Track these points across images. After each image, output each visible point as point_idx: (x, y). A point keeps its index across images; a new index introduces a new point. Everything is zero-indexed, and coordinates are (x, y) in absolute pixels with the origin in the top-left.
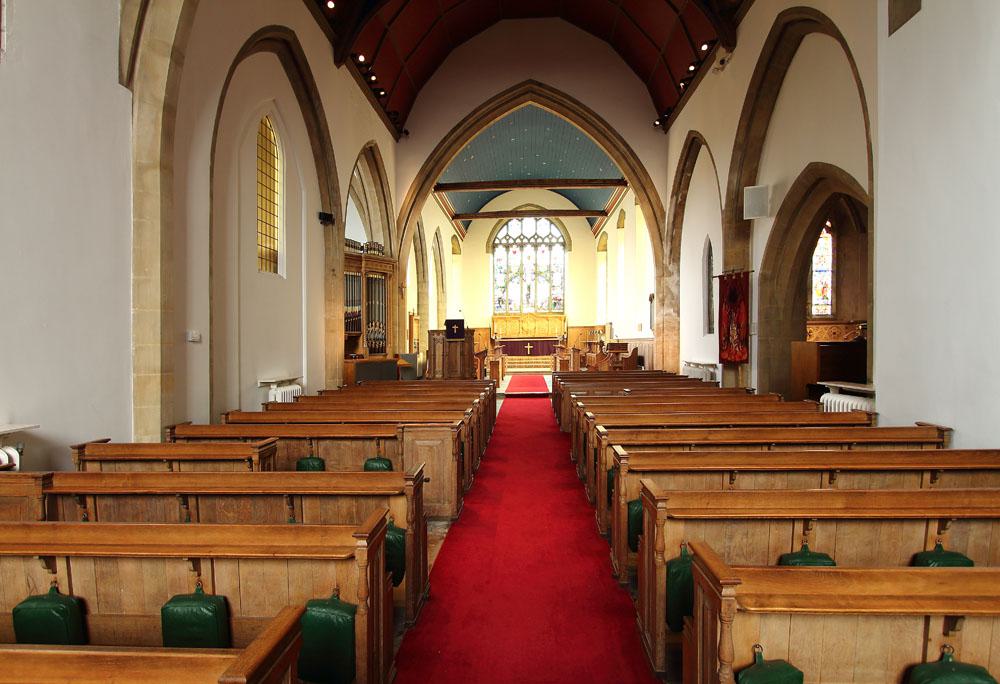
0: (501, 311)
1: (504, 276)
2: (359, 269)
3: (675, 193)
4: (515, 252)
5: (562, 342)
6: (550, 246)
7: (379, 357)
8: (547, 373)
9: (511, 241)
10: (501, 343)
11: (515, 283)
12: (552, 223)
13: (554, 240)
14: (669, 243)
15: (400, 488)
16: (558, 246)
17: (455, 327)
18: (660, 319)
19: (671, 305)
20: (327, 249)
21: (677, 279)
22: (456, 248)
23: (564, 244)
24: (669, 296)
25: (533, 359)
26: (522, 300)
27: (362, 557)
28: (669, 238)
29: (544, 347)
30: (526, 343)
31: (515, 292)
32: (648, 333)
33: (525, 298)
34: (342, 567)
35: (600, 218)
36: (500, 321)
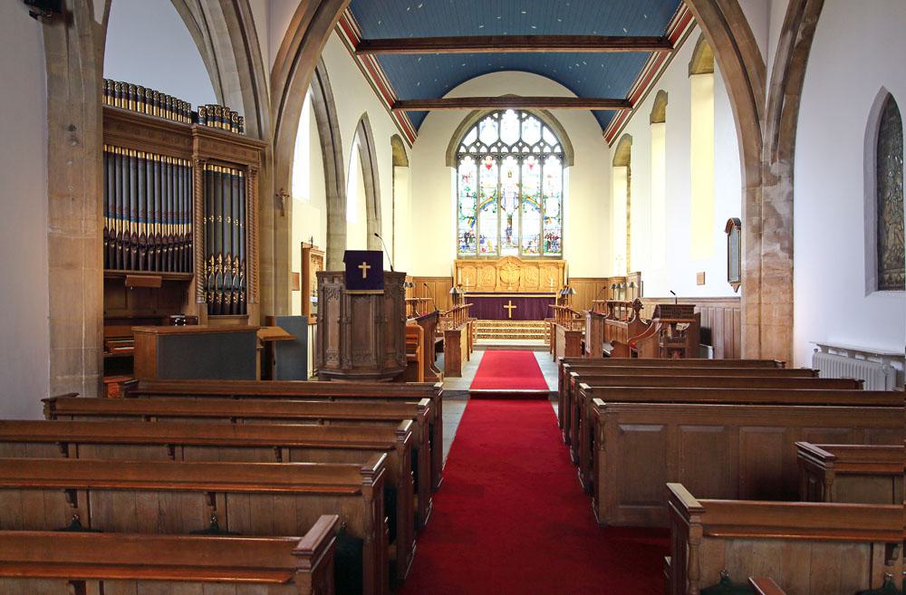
0: (468, 253)
1: (472, 201)
2: (187, 154)
3: (790, 25)
4: (489, 167)
5: (562, 301)
6: (542, 158)
7: (232, 322)
8: (539, 348)
9: (483, 150)
10: (468, 300)
11: (490, 211)
12: (544, 124)
13: (547, 150)
14: (773, 124)
15: (357, 486)
16: (553, 158)
17: (364, 267)
18: (755, 264)
19: (777, 237)
20: (54, 80)
21: (788, 189)
22: (400, 155)
23: (561, 156)
24: (772, 221)
25: (517, 325)
26: (499, 235)
27: (368, 494)
28: (774, 114)
29: (533, 307)
30: (505, 301)
31: (489, 225)
32: (719, 287)
33: (504, 234)
34: (352, 501)
35: (620, 111)
36: (467, 268)
